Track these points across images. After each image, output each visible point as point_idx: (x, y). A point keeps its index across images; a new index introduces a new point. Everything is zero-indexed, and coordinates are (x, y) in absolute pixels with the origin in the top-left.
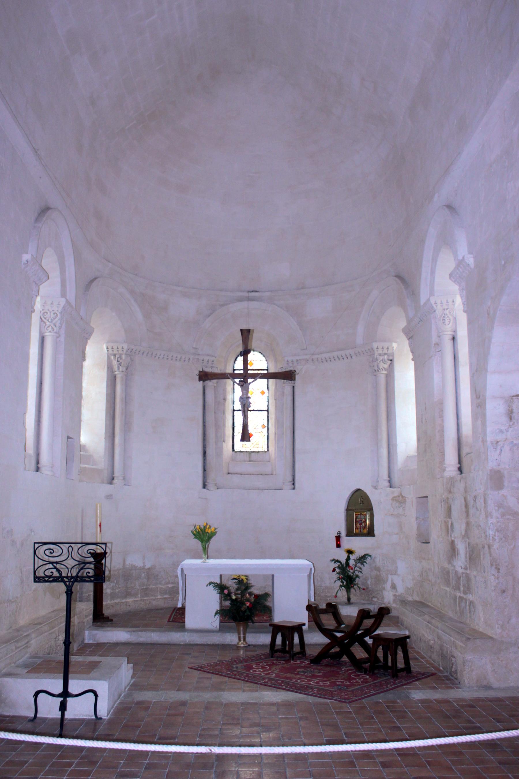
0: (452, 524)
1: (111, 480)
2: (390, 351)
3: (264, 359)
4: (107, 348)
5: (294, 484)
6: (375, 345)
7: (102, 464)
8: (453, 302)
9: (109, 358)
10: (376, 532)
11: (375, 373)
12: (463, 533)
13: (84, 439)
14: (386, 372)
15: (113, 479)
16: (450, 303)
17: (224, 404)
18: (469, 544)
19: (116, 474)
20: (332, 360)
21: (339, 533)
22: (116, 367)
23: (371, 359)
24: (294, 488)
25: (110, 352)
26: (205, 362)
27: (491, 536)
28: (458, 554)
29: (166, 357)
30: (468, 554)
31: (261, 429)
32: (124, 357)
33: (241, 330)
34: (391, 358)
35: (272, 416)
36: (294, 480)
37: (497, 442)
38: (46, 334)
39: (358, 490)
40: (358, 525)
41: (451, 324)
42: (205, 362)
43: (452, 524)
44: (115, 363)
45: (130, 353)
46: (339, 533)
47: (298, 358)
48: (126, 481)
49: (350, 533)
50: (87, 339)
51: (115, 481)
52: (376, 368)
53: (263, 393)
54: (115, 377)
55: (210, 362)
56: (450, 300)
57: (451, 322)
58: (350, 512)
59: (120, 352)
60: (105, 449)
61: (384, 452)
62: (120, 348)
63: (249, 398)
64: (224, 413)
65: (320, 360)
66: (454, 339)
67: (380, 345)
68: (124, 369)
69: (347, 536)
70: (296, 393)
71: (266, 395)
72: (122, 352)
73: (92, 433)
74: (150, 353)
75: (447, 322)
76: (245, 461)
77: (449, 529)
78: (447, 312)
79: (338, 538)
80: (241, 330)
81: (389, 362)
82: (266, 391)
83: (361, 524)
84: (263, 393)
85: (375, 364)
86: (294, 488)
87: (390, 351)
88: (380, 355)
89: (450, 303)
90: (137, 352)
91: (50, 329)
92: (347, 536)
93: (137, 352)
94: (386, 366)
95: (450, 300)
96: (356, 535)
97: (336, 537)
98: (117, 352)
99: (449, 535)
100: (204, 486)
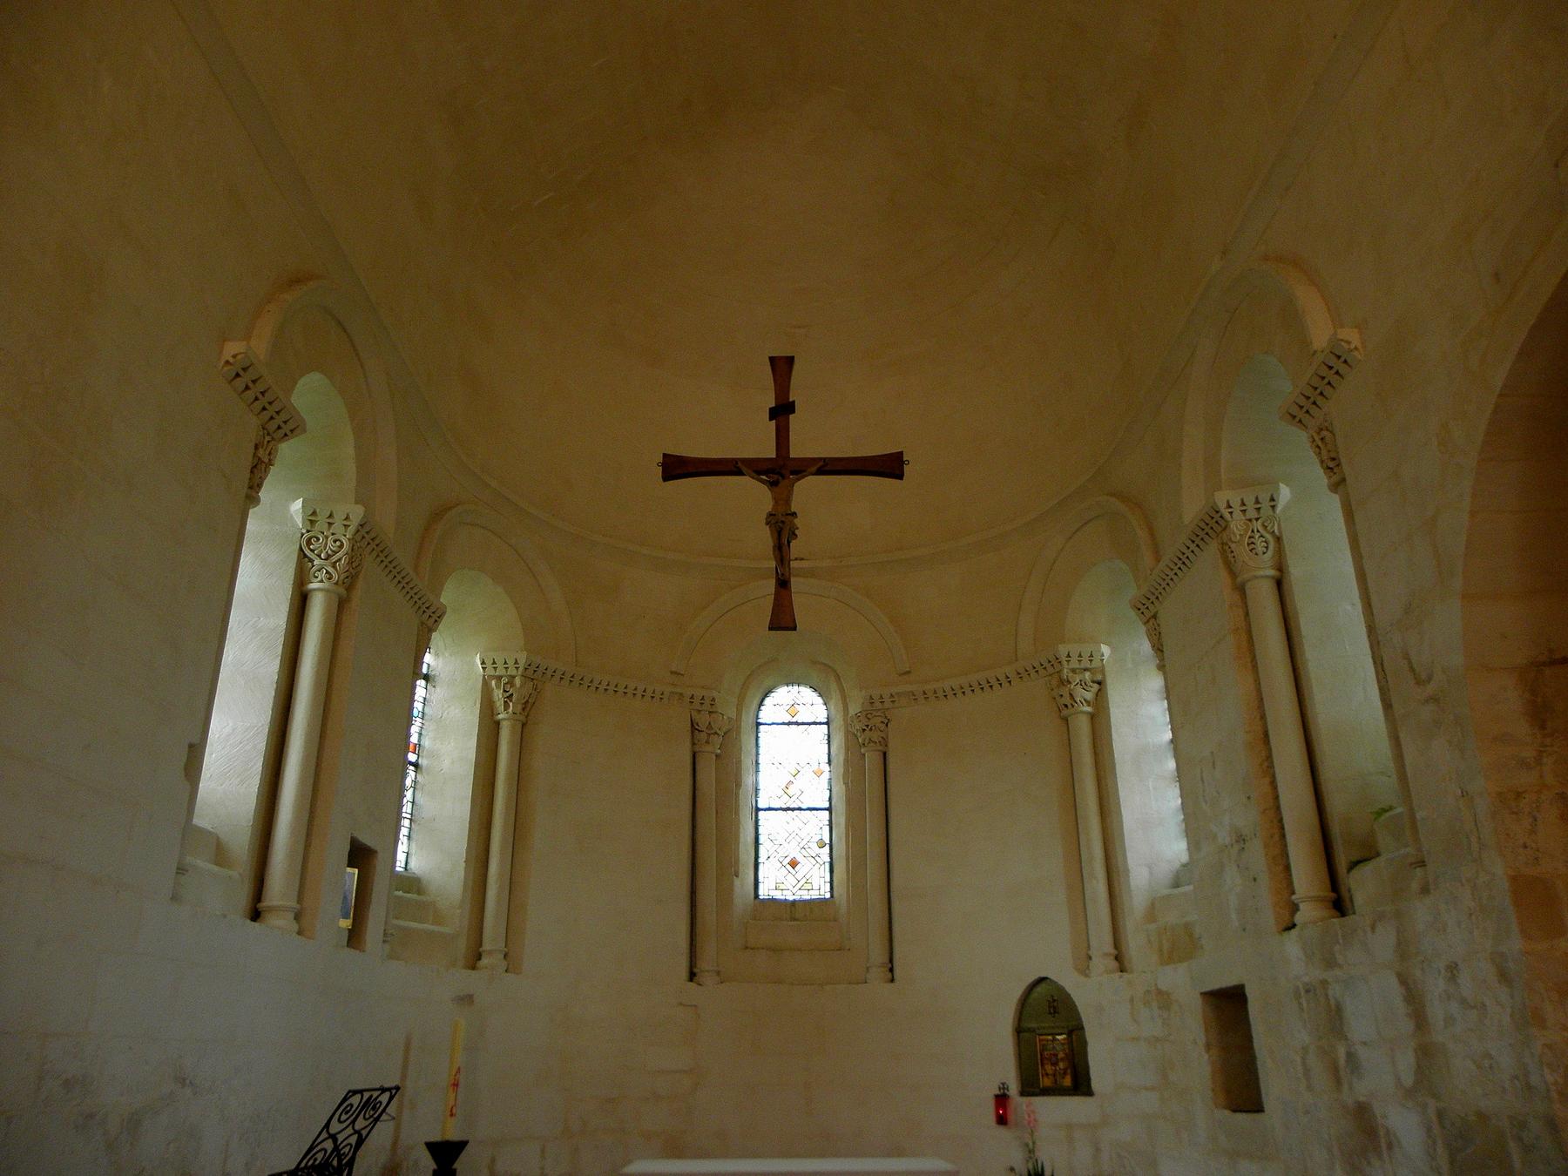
0: (1350, 1056)
1: (474, 958)
2: (1096, 663)
3: (820, 700)
4: (483, 663)
5: (891, 970)
6: (1063, 650)
7: (457, 922)
8: (1272, 499)
9: (486, 683)
10: (1095, 1085)
11: (1065, 712)
12: (1408, 1080)
13: (408, 855)
14: (1089, 709)
15: (479, 957)
16: (1265, 505)
17: (737, 795)
18: (1440, 1114)
19: (487, 946)
20: (968, 690)
21: (1004, 1086)
22: (500, 705)
23: (1054, 682)
24: (892, 980)
25: (490, 671)
26: (697, 701)
27: (1553, 1088)
28: (1390, 1146)
29: (611, 688)
30: (1440, 1149)
31: (815, 849)
32: (518, 681)
33: (772, 359)
34: (1099, 677)
35: (840, 820)
36: (891, 961)
37: (1519, 795)
38: (312, 586)
40: (1049, 1068)
41: (1270, 553)
42: (697, 701)
43: (1350, 1056)
44: (498, 695)
45: (533, 674)
46: (1004, 1086)
47: (894, 690)
48: (511, 962)
49: (1030, 1087)
50: (431, 630)
51: (485, 961)
52: (1067, 700)
53: (819, 774)
54: (498, 723)
55: (707, 702)
56: (1264, 498)
57: (1271, 547)
58: (1026, 1035)
60: (465, 890)
61: (1097, 886)
62: (511, 663)
63: (794, 514)
64: (737, 813)
65: (940, 694)
66: (1279, 584)
67: (1074, 649)
68: (520, 707)
69: (1023, 1093)
70: (891, 759)
71: (826, 776)
72: (514, 672)
73: (429, 839)
74: (577, 678)
75: (1260, 547)
76: (782, 411)
77: (1343, 1069)
78: (1258, 525)
79: (1002, 1100)
80: (772, 359)
81: (1096, 686)
82: (827, 768)
83: (1055, 1064)
84: (819, 774)
85: (1065, 691)
86: (892, 980)
87: (1096, 663)
88: (1074, 671)
89: (1265, 505)
90: (549, 673)
91: (322, 575)
92: (1023, 1093)
93: (549, 673)
94: (1089, 696)
95: (1264, 498)
96: (1045, 1092)
97: (997, 1096)
98: (503, 672)
99: (1345, 1087)
100: (692, 976)
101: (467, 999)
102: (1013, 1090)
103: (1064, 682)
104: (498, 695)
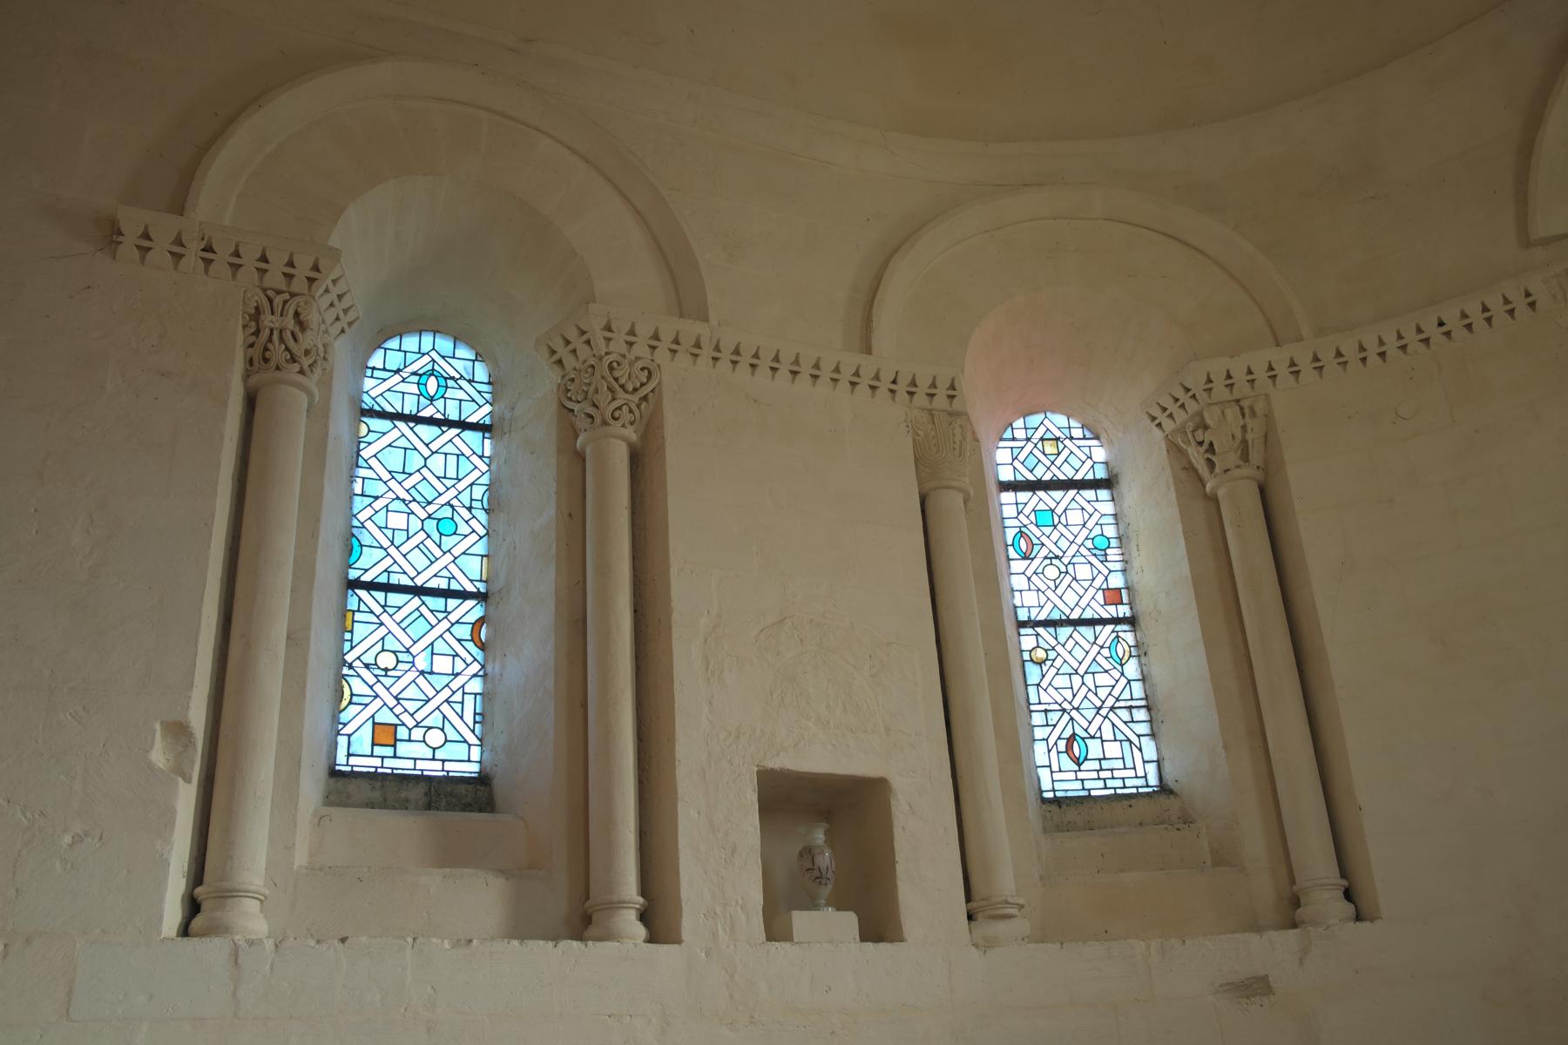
9: (1175, 450)
25: (1168, 425)
44: (1197, 457)
54: (1213, 500)
59: (1192, 407)
68: (1233, 459)
101: (1254, 987)
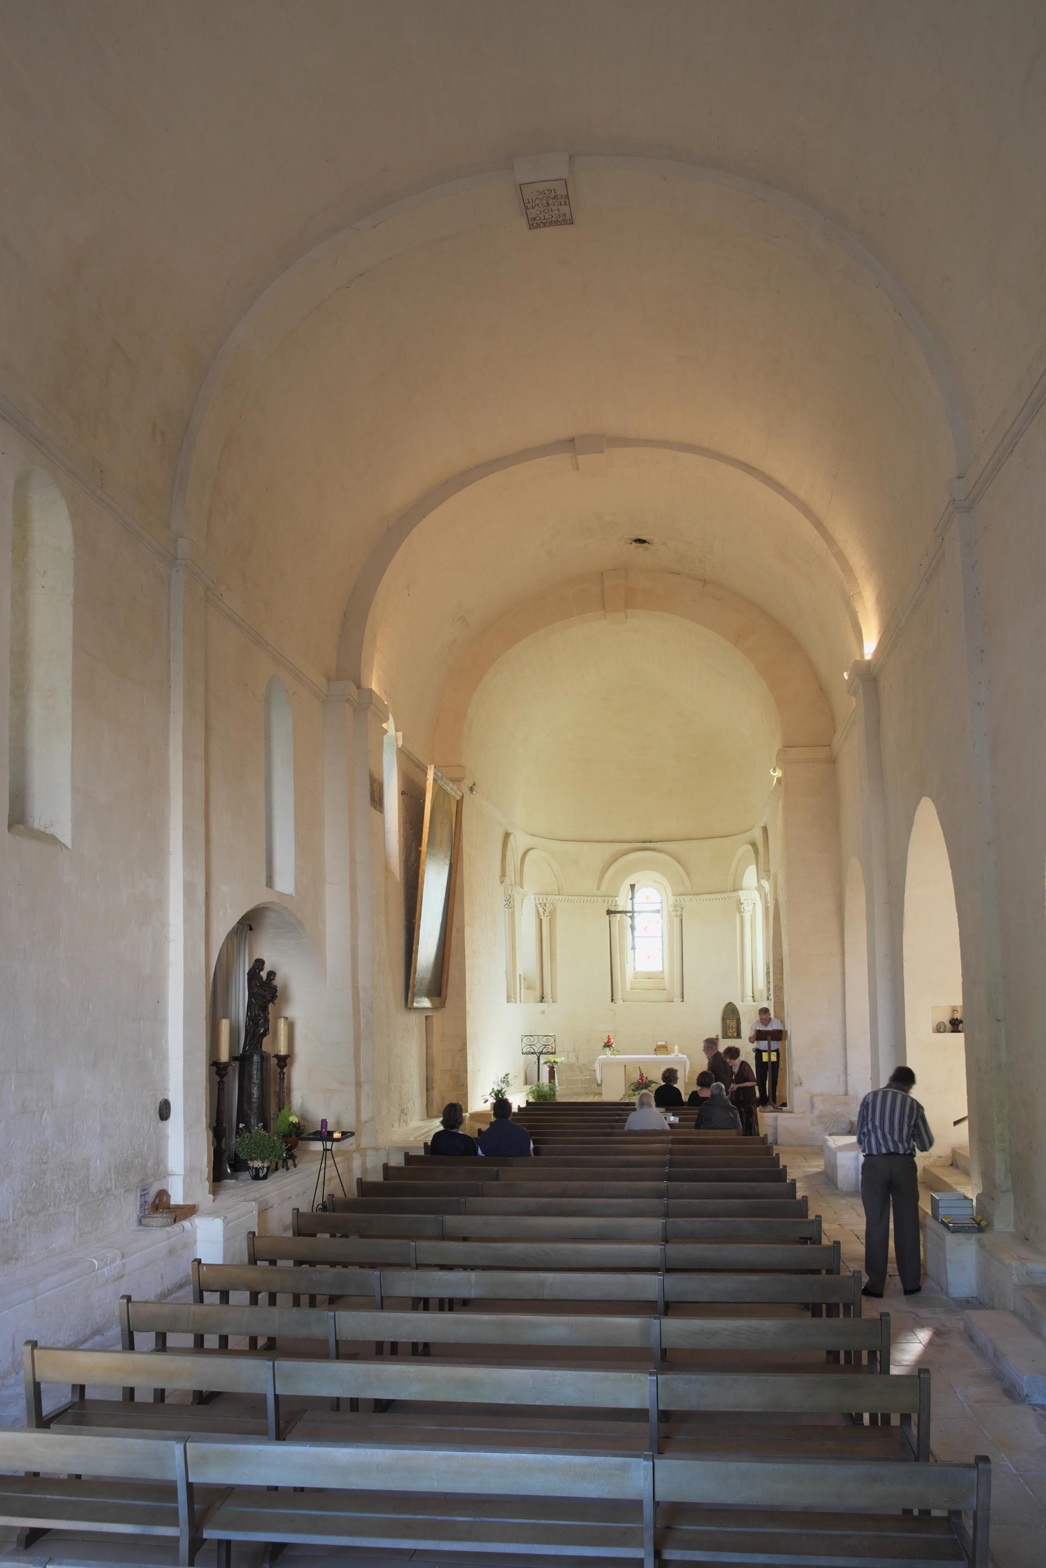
39: (730, 1003)
44: (541, 910)
96: (730, 1038)
101: (543, 1012)
102: (720, 1037)
103: (741, 904)
104: (541, 910)
